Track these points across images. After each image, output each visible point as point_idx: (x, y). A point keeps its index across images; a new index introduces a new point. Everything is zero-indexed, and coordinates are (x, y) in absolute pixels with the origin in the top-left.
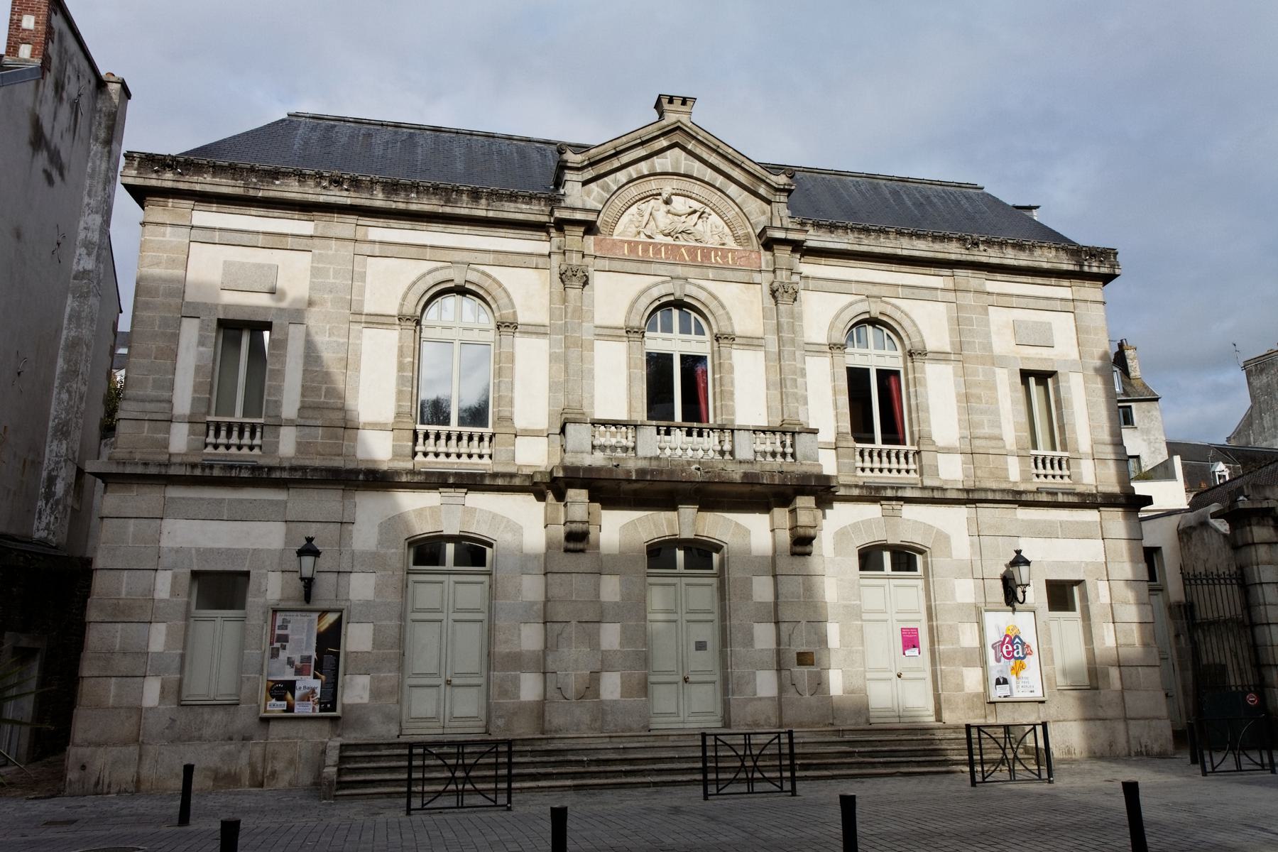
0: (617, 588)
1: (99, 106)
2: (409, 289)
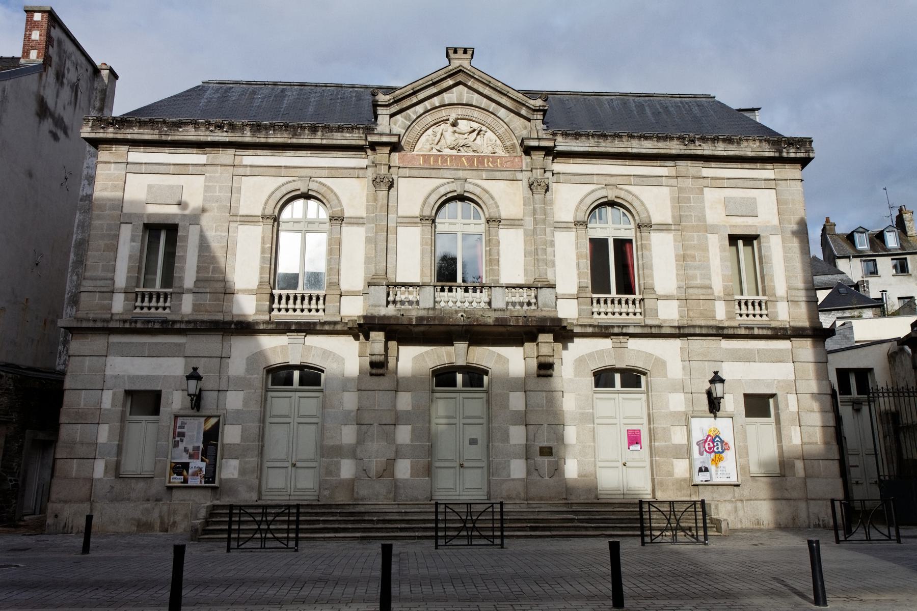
0: (410, 401)
1: (96, 86)
2: (270, 197)
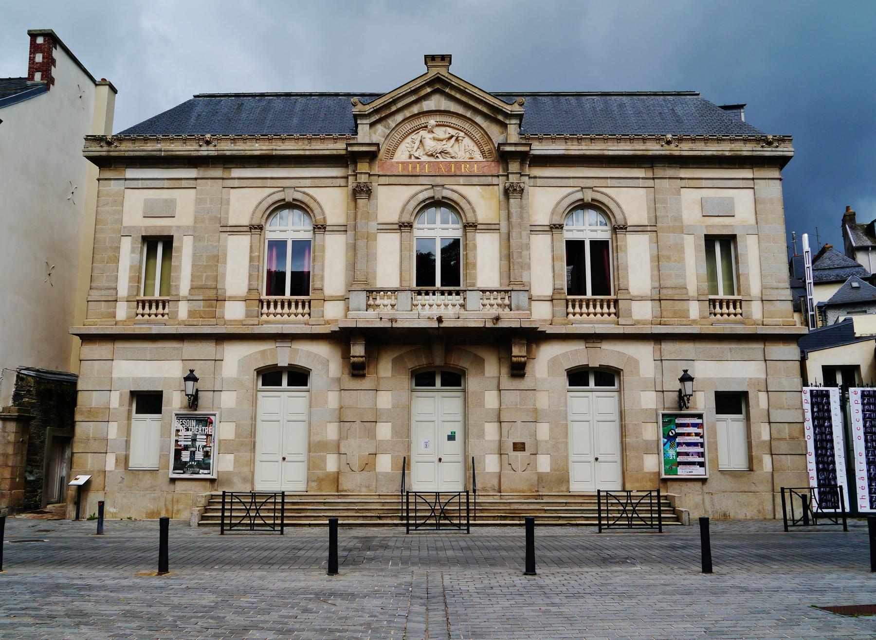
2: (257, 207)
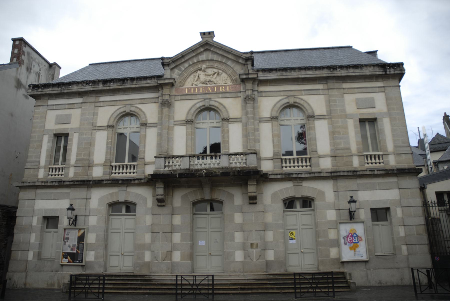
2: (111, 116)
